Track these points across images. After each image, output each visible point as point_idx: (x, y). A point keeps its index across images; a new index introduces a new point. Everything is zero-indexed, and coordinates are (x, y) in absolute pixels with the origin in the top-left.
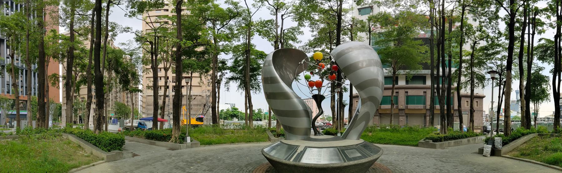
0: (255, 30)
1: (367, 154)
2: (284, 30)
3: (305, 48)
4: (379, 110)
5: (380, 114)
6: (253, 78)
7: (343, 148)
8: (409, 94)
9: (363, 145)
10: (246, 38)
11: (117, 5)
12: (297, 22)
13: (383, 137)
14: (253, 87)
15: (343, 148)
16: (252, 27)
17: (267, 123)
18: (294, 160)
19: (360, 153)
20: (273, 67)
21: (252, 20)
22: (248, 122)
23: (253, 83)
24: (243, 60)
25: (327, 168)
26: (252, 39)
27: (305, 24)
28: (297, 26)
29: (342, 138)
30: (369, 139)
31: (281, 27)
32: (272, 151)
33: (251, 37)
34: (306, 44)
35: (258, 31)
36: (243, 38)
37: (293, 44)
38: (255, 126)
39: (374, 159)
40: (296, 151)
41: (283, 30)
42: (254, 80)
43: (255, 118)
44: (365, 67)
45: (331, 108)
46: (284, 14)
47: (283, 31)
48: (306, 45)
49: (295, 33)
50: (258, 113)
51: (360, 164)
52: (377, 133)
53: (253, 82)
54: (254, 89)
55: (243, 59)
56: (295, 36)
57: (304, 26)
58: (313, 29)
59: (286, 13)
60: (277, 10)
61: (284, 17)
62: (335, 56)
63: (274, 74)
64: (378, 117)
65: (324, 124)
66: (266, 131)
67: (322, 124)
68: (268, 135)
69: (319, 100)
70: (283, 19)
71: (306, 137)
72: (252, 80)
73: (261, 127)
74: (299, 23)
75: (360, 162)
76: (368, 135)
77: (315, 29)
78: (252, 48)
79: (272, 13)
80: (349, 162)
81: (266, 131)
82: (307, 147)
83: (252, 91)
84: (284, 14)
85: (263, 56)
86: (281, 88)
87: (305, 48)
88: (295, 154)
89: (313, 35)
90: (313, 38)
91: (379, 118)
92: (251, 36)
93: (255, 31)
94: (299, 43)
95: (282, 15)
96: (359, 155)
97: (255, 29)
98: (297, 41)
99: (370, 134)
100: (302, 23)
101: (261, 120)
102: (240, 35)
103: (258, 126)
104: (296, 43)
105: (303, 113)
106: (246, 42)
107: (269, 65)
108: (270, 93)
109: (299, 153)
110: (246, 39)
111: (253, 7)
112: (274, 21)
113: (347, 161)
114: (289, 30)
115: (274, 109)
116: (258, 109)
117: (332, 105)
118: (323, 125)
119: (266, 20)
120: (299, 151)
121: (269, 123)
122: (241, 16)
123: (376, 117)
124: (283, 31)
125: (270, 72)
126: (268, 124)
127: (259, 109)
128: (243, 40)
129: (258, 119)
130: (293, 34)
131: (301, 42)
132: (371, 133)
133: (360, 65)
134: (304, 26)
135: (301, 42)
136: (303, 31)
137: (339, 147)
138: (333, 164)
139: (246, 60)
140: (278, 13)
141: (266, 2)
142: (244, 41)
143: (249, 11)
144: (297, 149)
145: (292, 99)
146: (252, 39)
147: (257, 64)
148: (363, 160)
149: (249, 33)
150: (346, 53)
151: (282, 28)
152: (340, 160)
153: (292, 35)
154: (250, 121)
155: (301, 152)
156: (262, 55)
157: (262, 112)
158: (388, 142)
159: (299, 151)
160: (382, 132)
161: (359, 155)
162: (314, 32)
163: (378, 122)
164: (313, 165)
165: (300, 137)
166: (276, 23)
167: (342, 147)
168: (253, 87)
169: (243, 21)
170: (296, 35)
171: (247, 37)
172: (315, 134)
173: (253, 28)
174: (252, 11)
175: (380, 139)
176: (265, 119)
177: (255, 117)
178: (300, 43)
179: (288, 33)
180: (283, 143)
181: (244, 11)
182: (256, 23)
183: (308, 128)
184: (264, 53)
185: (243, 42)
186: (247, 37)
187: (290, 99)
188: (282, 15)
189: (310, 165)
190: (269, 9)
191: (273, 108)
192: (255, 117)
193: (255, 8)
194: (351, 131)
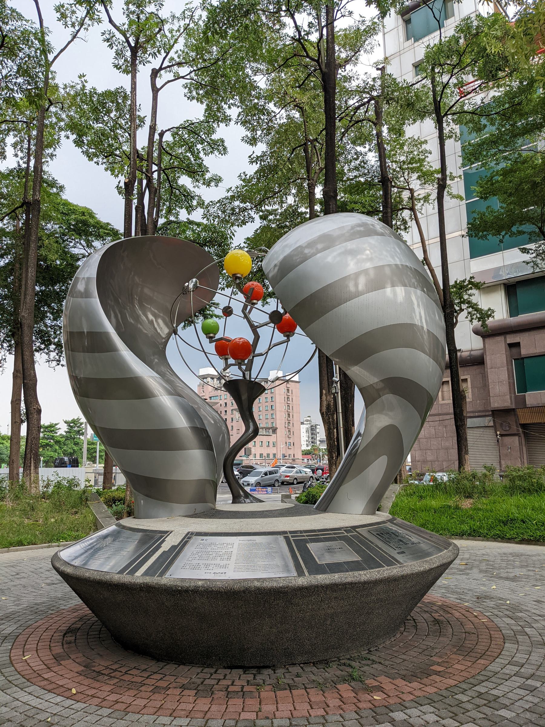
0: (63, 120)
1: (393, 558)
2: (161, 135)
3: (229, 207)
4: (519, 412)
5: (524, 426)
6: (49, 306)
7: (303, 536)
8: (524, 351)
9: (376, 530)
10: (29, 149)
11: (224, 679)
12: (202, 103)
13: (515, 513)
14: (47, 342)
15: (303, 536)
16: (53, 109)
17: (99, 474)
18: (146, 573)
19: (358, 551)
20: (96, 302)
21: (53, 78)
22: (21, 470)
23: (46, 326)
24: (12, 235)
25: (244, 592)
26: (49, 159)
27: (228, 112)
28: (202, 118)
29: (316, 508)
30: (463, 522)
31: (148, 122)
32: (92, 555)
33: (49, 151)
34: (230, 194)
35: (73, 127)
36: (15, 145)
37: (192, 189)
38: (47, 486)
39: (405, 573)
40: (159, 547)
41: (159, 131)
42: (52, 313)
43: (52, 454)
44: (362, 293)
45: (322, 414)
46: (161, 69)
47: (157, 137)
48: (233, 198)
49: (199, 146)
50: (67, 438)
51: (351, 584)
52: (491, 498)
53: (48, 322)
54: (52, 347)
55: (11, 228)
56: (197, 157)
57: (227, 120)
58: (254, 130)
59: (166, 64)
60: (134, 51)
61: (159, 83)
62: (278, 264)
63: (101, 324)
64: (517, 438)
65: (314, 471)
66: (87, 500)
67: (308, 470)
68: (93, 514)
69: (244, 397)
70: (155, 90)
71: (200, 507)
72: (43, 317)
73: (69, 488)
74: (209, 109)
75: (349, 580)
76: (457, 508)
77: (259, 133)
78: (49, 195)
79: (121, 62)
80: (312, 576)
81: (87, 500)
82: (192, 533)
83: (44, 356)
84: (161, 69)
85: (89, 226)
86: (122, 365)
87: (229, 207)
88: (153, 555)
89: (254, 155)
90: (255, 167)
91: (520, 444)
92: (49, 146)
93: (62, 124)
94: (213, 184)
95: (155, 73)
96: (356, 558)
97: (64, 116)
98: (208, 176)
99: (466, 504)
100: (220, 109)
101: (75, 463)
102: (7, 135)
103: (59, 485)
104: (204, 184)
105: (189, 437)
106: (28, 166)
107: (87, 294)
108: (88, 380)
109: (164, 551)
110: (29, 155)
111: (59, 20)
112: (125, 97)
113: (306, 573)
114: (177, 134)
115: (101, 428)
116: (70, 419)
117: (325, 403)
118: (311, 474)
119: (99, 91)
120: (166, 547)
121: (105, 474)
122: (12, 53)
123: (507, 440)
124: (157, 137)
125: (91, 316)
126: (101, 479)
127: (73, 421)
128: (16, 155)
129: (66, 459)
130: (190, 149)
131: (217, 180)
132: (471, 501)
133: (352, 287)
134: (227, 120)
135: (217, 180)
136: (222, 141)
137: (291, 532)
138: (264, 580)
139: (24, 237)
140: (140, 67)
141: (99, 7)
142: (21, 162)
143: (42, 41)
144: (163, 541)
145: (154, 396)
146: (52, 156)
147: (65, 254)
148: (361, 572)
149: (41, 128)
150: (305, 258)
151: (153, 129)
152: (286, 568)
153: (189, 154)
154: (26, 467)
155: (173, 548)
156: (85, 223)
157: (83, 434)
158: (539, 533)
159: (166, 547)
160: (514, 498)
161: (356, 558)
162: (259, 144)
163: (521, 457)
164: (200, 583)
165: (182, 508)
166: (133, 109)
167: (301, 532)
168: (49, 340)
169: (20, 80)
170: (202, 155)
171: (33, 148)
172: (236, 499)
173: (56, 114)
174: (53, 44)
175: (505, 523)
176: (92, 459)
177: (55, 451)
178: (217, 186)
179: (174, 144)
180: (124, 527)
181: (25, 36)
182: (68, 94)
183: (208, 481)
184: (91, 215)
185: (15, 165)
186: (33, 148)
187: (156, 396)
188: (155, 73)
189: (193, 584)
190: (111, 46)
191: (97, 425)
192: (55, 451)
193: (66, 25)
194: (342, 487)
